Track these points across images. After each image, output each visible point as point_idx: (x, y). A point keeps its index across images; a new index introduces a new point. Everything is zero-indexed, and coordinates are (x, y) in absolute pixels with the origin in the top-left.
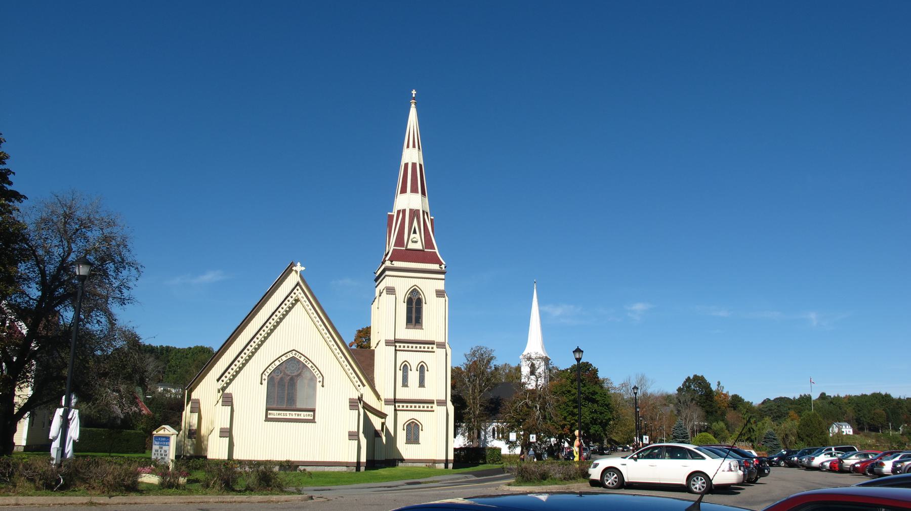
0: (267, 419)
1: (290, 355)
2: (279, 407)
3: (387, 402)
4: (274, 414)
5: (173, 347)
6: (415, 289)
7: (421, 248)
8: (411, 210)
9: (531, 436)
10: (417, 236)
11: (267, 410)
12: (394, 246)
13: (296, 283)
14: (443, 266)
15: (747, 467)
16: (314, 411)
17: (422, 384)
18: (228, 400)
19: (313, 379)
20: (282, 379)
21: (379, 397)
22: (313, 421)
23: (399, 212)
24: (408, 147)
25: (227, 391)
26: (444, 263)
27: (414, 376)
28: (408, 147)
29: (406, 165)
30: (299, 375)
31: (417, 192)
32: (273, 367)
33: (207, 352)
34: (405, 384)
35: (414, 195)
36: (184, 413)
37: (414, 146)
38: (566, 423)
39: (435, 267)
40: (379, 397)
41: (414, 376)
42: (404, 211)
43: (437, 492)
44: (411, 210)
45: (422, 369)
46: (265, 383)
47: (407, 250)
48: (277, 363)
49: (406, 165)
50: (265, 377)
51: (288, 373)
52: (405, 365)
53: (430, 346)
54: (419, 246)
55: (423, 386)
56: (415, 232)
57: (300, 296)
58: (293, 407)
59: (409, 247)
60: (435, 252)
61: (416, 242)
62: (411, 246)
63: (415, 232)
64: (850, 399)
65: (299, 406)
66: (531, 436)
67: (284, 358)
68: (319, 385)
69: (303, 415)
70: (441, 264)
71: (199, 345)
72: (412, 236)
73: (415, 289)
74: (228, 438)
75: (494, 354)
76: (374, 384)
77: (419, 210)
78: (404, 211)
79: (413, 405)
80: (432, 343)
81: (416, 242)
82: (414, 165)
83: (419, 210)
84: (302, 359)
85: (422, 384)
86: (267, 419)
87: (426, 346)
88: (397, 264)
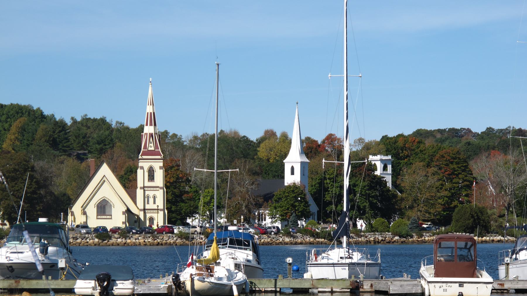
0: (97, 219)
1: (103, 199)
2: (101, 214)
3: (141, 210)
4: (99, 217)
7: (153, 149)
8: (150, 133)
10: (152, 145)
11: (97, 215)
12: (143, 149)
13: (103, 176)
14: (162, 157)
15: (358, 231)
16: (111, 215)
17: (154, 203)
18: (85, 213)
19: (111, 206)
20: (101, 206)
22: (111, 219)
23: (145, 134)
24: (148, 105)
26: (162, 155)
27: (151, 200)
28: (148, 105)
29: (148, 113)
30: (106, 204)
31: (152, 125)
32: (98, 202)
33: (26, 112)
34: (148, 203)
35: (151, 127)
36: (68, 216)
37: (151, 105)
38: (289, 211)
39: (159, 157)
41: (151, 200)
42: (147, 134)
44: (150, 133)
45: (154, 198)
46: (96, 207)
47: (148, 150)
48: (99, 201)
49: (148, 113)
50: (96, 205)
51: (103, 204)
52: (155, 196)
53: (158, 188)
54: (153, 149)
55: (149, 204)
56: (151, 143)
57: (105, 180)
58: (105, 215)
59: (149, 149)
60: (159, 151)
61: (152, 147)
62: (150, 149)
63: (151, 143)
65: (107, 214)
66: (234, 221)
67: (101, 200)
68: (113, 207)
69: (108, 217)
70: (161, 155)
71: (15, 102)
72: (150, 144)
73: (151, 167)
77: (153, 133)
78: (147, 134)
79: (153, 211)
80: (158, 187)
81: (152, 147)
82: (151, 113)
83: (153, 133)
84: (107, 199)
85: (154, 203)
86: (97, 219)
87: (156, 188)
88: (144, 157)
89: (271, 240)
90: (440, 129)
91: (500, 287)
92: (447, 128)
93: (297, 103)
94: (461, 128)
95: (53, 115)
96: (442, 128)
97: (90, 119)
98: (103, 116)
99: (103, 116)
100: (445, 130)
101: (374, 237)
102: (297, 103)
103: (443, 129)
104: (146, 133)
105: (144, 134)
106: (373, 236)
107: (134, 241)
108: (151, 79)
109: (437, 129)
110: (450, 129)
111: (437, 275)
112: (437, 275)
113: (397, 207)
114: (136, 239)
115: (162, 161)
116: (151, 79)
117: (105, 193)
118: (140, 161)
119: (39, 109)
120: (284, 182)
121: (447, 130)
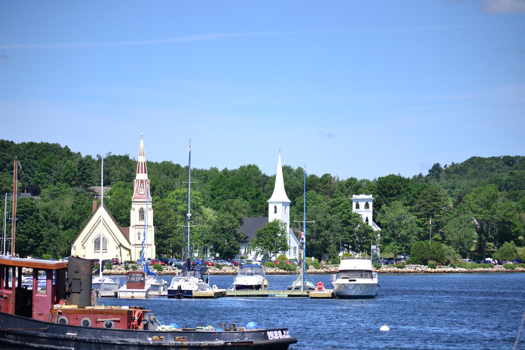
5: (10, 141)
6: (142, 208)
8: (141, 180)
9: (217, 254)
10: (143, 189)
11: (95, 250)
16: (107, 250)
21: (130, 243)
22: (106, 252)
23: (137, 180)
25: (84, 245)
31: (143, 173)
37: (142, 155)
40: (130, 243)
43: (250, 300)
44: (141, 180)
46: (94, 243)
50: (94, 241)
56: (142, 188)
64: (156, 249)
66: (217, 254)
68: (108, 243)
71: (45, 141)
72: (141, 189)
74: (93, 282)
75: (338, 175)
76: (129, 238)
77: (143, 180)
78: (138, 180)
82: (142, 163)
86: (95, 252)
89: (235, 271)
90: (494, 157)
91: (159, 294)
92: (502, 156)
93: (280, 150)
94: (516, 156)
95: (79, 153)
96: (497, 155)
97: (114, 156)
98: (126, 154)
99: (126, 154)
100: (500, 158)
101: (335, 269)
102: (280, 150)
103: (498, 156)
104: (138, 179)
105: (136, 180)
106: (334, 267)
107: (118, 271)
108: (142, 133)
109: (491, 156)
110: (505, 156)
111: (128, 288)
112: (128, 288)
113: (513, 234)
114: (119, 270)
115: (151, 203)
116: (142, 133)
117: (101, 231)
118: (132, 203)
119: (66, 147)
120: (268, 220)
121: (502, 158)
